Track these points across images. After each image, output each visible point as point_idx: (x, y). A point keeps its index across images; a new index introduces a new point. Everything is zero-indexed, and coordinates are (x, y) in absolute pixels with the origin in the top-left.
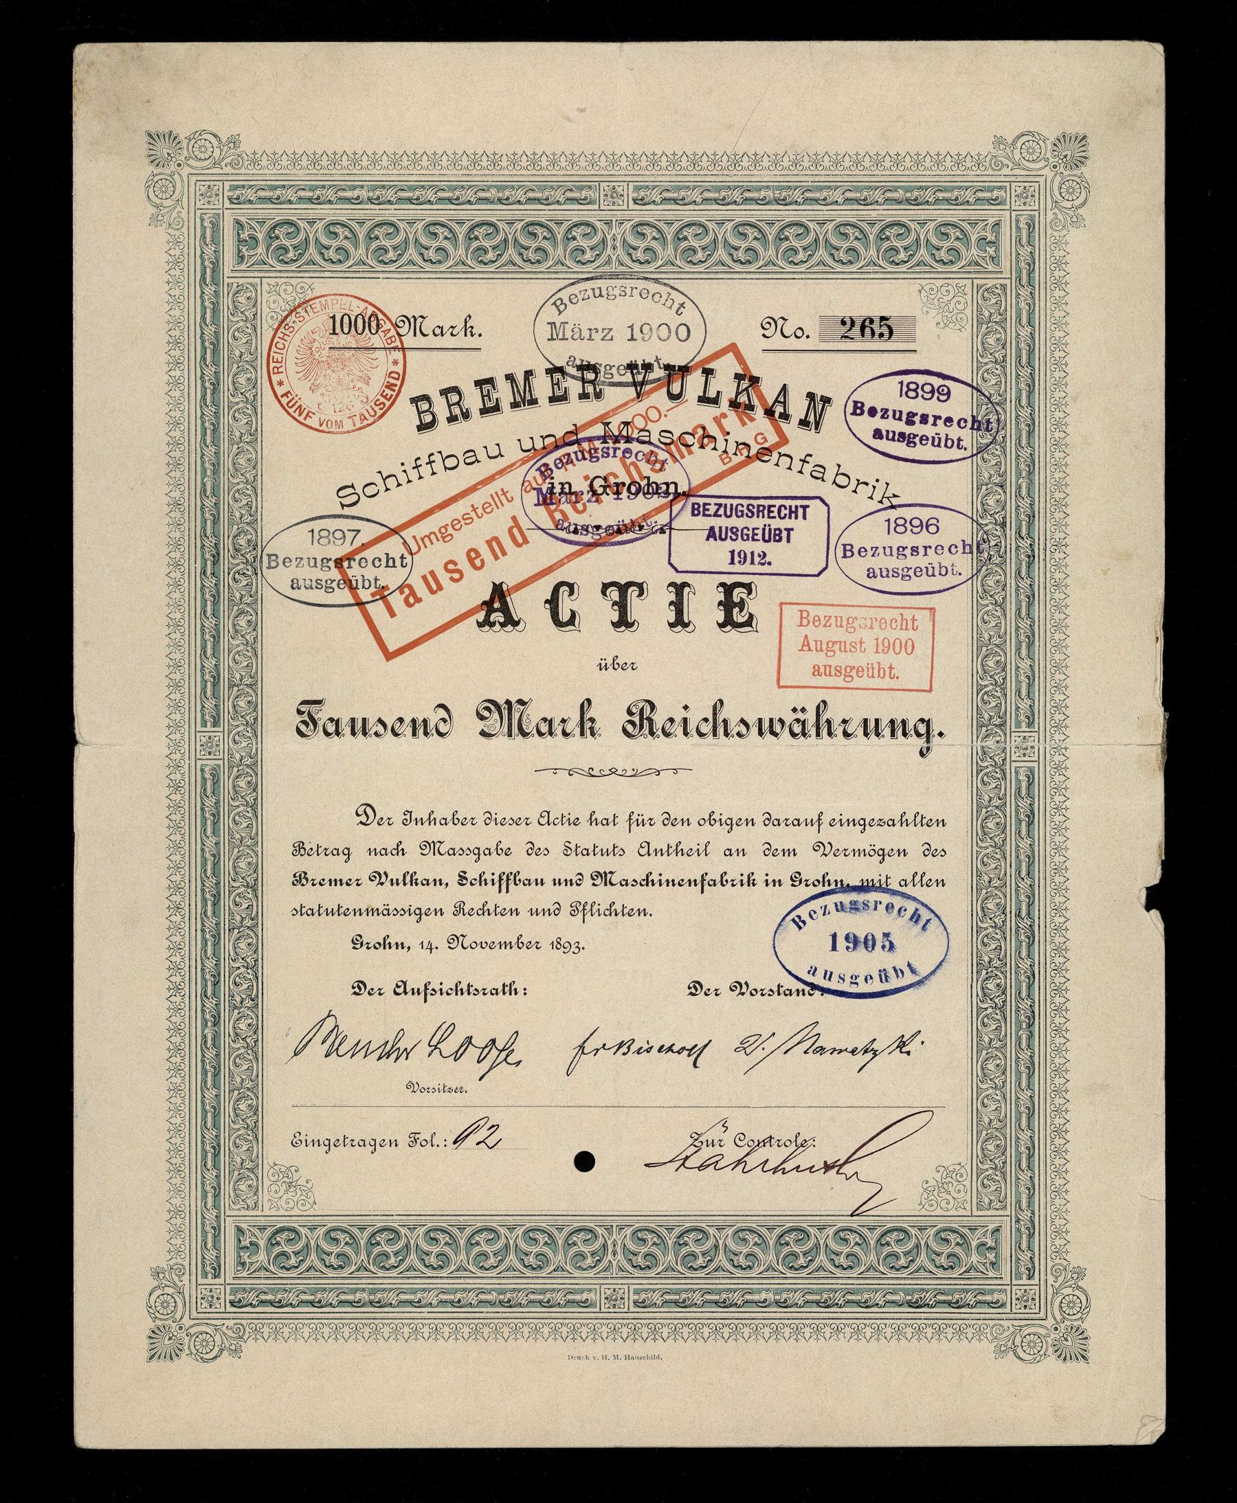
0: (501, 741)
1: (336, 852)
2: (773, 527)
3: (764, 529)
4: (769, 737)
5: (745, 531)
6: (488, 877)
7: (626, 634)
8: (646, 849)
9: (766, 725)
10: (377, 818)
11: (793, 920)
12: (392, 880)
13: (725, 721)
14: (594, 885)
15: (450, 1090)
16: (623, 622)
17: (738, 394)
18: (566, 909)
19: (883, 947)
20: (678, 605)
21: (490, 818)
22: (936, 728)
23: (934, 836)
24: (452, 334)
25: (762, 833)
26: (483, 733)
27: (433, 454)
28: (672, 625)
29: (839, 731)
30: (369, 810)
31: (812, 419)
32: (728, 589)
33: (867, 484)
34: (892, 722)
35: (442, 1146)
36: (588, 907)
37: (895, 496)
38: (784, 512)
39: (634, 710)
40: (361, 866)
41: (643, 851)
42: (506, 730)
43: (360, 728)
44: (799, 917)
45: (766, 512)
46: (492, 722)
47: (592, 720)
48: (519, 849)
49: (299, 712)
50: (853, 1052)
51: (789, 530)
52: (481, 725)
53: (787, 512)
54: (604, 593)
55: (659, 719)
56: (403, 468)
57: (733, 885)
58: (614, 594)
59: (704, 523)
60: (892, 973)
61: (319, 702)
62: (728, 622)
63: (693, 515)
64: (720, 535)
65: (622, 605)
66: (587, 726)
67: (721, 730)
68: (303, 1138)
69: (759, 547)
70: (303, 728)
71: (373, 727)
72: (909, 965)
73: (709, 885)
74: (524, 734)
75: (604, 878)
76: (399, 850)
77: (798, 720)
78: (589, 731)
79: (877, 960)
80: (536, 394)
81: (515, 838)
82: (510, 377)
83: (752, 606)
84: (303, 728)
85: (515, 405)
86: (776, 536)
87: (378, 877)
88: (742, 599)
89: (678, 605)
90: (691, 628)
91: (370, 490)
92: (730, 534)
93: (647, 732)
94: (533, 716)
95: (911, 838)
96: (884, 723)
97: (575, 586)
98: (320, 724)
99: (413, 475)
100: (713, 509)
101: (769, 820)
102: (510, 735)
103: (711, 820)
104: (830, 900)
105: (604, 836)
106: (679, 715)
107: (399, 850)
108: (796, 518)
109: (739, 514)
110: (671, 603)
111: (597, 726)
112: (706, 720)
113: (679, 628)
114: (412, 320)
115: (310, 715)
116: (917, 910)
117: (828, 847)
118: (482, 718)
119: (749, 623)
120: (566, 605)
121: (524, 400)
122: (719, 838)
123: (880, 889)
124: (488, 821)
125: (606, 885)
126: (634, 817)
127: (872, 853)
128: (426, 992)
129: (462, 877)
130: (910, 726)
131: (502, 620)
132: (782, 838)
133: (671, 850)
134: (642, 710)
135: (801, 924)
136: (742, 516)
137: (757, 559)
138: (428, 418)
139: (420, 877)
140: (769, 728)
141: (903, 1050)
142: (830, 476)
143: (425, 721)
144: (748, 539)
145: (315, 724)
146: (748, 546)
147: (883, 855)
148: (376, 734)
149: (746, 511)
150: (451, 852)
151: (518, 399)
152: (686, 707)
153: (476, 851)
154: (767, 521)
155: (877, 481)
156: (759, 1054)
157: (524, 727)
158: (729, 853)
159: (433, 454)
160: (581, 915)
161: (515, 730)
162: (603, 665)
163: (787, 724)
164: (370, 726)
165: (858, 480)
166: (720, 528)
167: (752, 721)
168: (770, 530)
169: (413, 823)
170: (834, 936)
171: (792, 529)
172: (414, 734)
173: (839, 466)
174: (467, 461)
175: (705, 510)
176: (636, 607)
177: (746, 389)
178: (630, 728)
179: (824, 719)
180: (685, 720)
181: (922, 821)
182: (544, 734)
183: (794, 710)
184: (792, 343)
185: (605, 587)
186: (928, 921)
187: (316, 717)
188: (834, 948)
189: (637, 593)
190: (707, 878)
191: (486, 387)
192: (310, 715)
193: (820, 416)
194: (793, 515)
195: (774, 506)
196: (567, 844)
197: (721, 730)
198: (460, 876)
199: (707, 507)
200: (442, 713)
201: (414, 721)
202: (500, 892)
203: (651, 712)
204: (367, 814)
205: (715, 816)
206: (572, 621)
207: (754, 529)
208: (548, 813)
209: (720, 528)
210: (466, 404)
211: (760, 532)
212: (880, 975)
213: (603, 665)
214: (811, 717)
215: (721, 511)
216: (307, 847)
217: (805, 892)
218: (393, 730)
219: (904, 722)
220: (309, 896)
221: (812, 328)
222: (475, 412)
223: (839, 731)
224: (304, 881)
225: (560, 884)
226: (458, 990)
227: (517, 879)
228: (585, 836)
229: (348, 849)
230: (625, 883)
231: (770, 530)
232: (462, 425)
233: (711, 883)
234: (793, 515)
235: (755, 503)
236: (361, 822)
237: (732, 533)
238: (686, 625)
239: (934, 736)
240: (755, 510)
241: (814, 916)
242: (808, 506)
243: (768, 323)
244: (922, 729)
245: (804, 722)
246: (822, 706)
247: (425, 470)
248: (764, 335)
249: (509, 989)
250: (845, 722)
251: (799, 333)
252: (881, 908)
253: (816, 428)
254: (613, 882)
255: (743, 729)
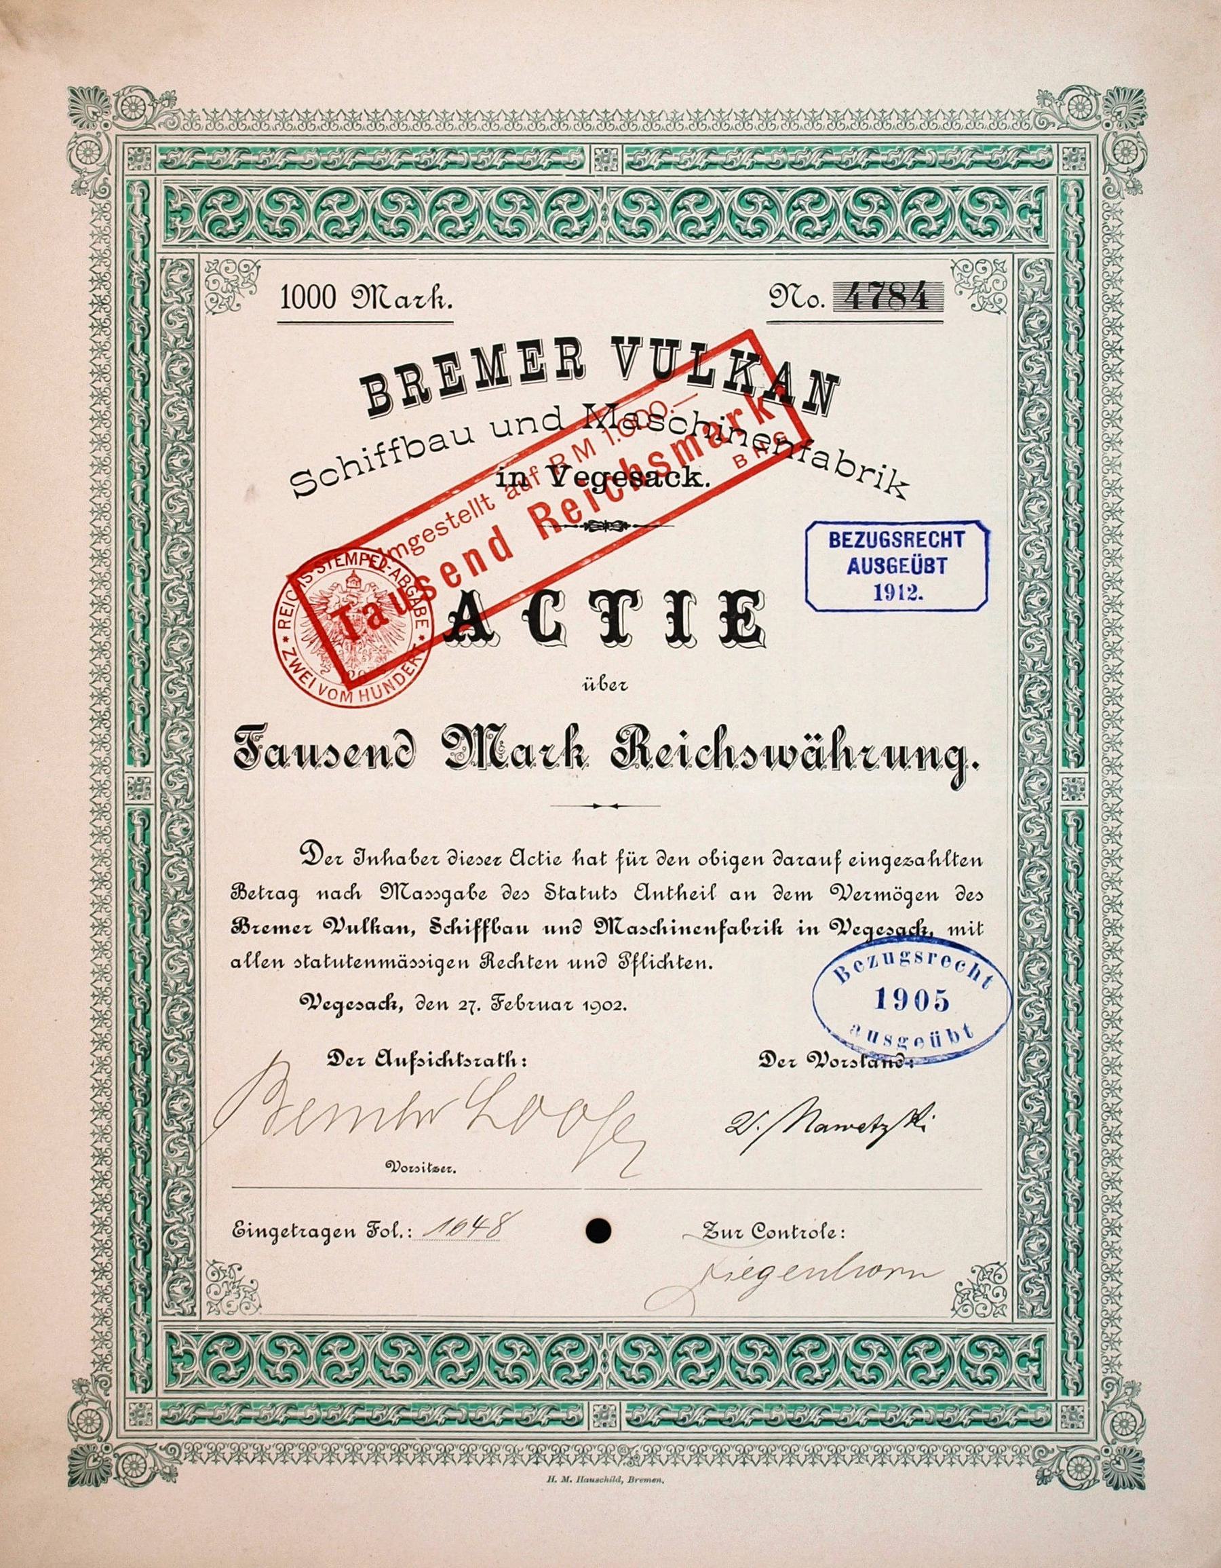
0: (471, 771)
1: (282, 895)
2: (923, 557)
3: (913, 561)
4: (778, 767)
5: (892, 563)
6: (461, 924)
7: (616, 649)
8: (644, 893)
9: (775, 754)
10: (325, 856)
11: (836, 972)
12: (350, 927)
13: (729, 750)
14: (598, 932)
15: (436, 1170)
16: (614, 636)
17: (734, 372)
18: (613, 961)
19: (937, 1006)
20: (677, 616)
21: (454, 857)
22: (969, 759)
23: (971, 878)
24: (418, 306)
25: (772, 874)
26: (450, 763)
27: (396, 439)
28: (670, 640)
29: (858, 760)
30: (315, 847)
31: (818, 401)
32: (732, 598)
33: (873, 471)
34: (920, 751)
35: (405, 1236)
36: (640, 959)
37: (903, 484)
38: (935, 539)
39: (624, 736)
40: (313, 911)
41: (641, 894)
42: (476, 760)
43: (307, 757)
44: (843, 968)
45: (915, 539)
46: (460, 750)
47: (579, 748)
48: (495, 893)
49: (238, 739)
50: (860, 1129)
51: (942, 560)
52: (447, 753)
53: (939, 538)
54: (592, 602)
55: (653, 747)
56: (365, 454)
57: (756, 933)
58: (605, 606)
59: (844, 555)
60: (944, 1037)
61: (261, 727)
62: (732, 635)
63: (832, 546)
64: (864, 566)
65: (613, 617)
66: (574, 755)
67: (723, 759)
68: (246, 1227)
69: (908, 579)
70: (242, 757)
71: (323, 756)
72: (965, 1028)
73: (730, 933)
74: (498, 764)
75: (608, 924)
76: (354, 893)
77: (812, 749)
78: (575, 760)
79: (931, 1020)
80: (506, 373)
81: (485, 878)
82: (476, 352)
83: (758, 617)
84: (242, 757)
85: (481, 384)
86: (928, 566)
87: (333, 924)
88: (747, 610)
89: (677, 616)
90: (691, 643)
91: (329, 478)
92: (874, 566)
93: (639, 761)
94: (508, 743)
95: (944, 879)
96: (911, 752)
97: (561, 595)
98: (262, 752)
99: (376, 461)
100: (854, 539)
101: (782, 859)
102: (481, 764)
103: (713, 859)
104: (878, 950)
105: (593, 878)
106: (676, 743)
107: (354, 893)
108: (950, 545)
109: (885, 543)
110: (669, 615)
111: (584, 755)
112: (707, 748)
113: (679, 642)
114: (371, 290)
115: (250, 743)
116: (976, 965)
117: (847, 889)
118: (448, 745)
119: (755, 637)
120: (549, 618)
121: (493, 378)
122: (722, 873)
123: (910, 938)
124: (453, 860)
125: (611, 932)
126: (624, 855)
127: (898, 896)
128: (413, 1061)
129: (435, 925)
130: (940, 756)
131: (472, 633)
132: (794, 878)
133: (672, 893)
134: (633, 736)
135: (844, 977)
136: (888, 545)
137: (906, 594)
138: (381, 401)
139: (382, 923)
140: (778, 758)
141: (917, 1124)
142: (832, 465)
143: (933, 751)
144: (896, 571)
145: (256, 752)
146: (896, 579)
147: (910, 899)
148: (745, 765)
149: (892, 540)
150: (417, 895)
151: (486, 377)
152: (683, 733)
153: (446, 895)
154: (917, 550)
155: (884, 466)
156: (752, 1133)
157: (498, 756)
158: (735, 896)
159: (396, 439)
160: (631, 966)
161: (487, 758)
162: (589, 685)
163: (800, 752)
164: (320, 754)
165: (863, 467)
166: (864, 559)
167: (759, 749)
168: (921, 560)
169: (367, 862)
170: (882, 991)
171: (946, 559)
172: (371, 764)
173: (842, 452)
174: (434, 447)
175: (845, 539)
176: (629, 619)
177: (744, 368)
178: (619, 757)
179: (842, 748)
180: (683, 748)
181: (952, 859)
182: (521, 764)
183: (808, 737)
184: (805, 313)
185: (594, 596)
186: (989, 978)
187: (257, 744)
188: (881, 1006)
189: (630, 602)
190: (727, 925)
191: (447, 364)
192: (250, 743)
193: (827, 397)
194: (946, 543)
195: (925, 533)
196: (550, 886)
197: (723, 759)
198: (432, 922)
199: (847, 536)
200: (403, 740)
201: (370, 749)
202: (476, 940)
203: (645, 737)
204: (312, 851)
205: (719, 854)
206: (556, 635)
207: (901, 560)
208: (522, 851)
209: (864, 559)
210: (425, 383)
211: (909, 563)
212: (932, 1038)
213: (589, 685)
214: (826, 745)
215: (864, 542)
216: (248, 889)
217: (851, 940)
218: (346, 758)
219: (933, 751)
220: (247, 942)
221: (827, 297)
222: (435, 393)
223: (858, 760)
224: (245, 928)
225: (553, 932)
226: (445, 1060)
227: (746, 926)
228: (569, 876)
229: (296, 892)
230: (633, 930)
231: (921, 560)
232: (420, 408)
233: (732, 930)
234: (946, 543)
235: (903, 529)
236: (306, 862)
237: (877, 564)
238: (685, 640)
239: (967, 767)
240: (903, 539)
241: (860, 967)
242: (963, 532)
243: (779, 291)
244: (954, 759)
245: (818, 751)
246: (839, 732)
247: (389, 457)
248: (773, 305)
249: (506, 1059)
250: (865, 750)
251: (813, 301)
252: (937, 961)
253: (823, 411)
254: (620, 929)
255: (749, 759)
